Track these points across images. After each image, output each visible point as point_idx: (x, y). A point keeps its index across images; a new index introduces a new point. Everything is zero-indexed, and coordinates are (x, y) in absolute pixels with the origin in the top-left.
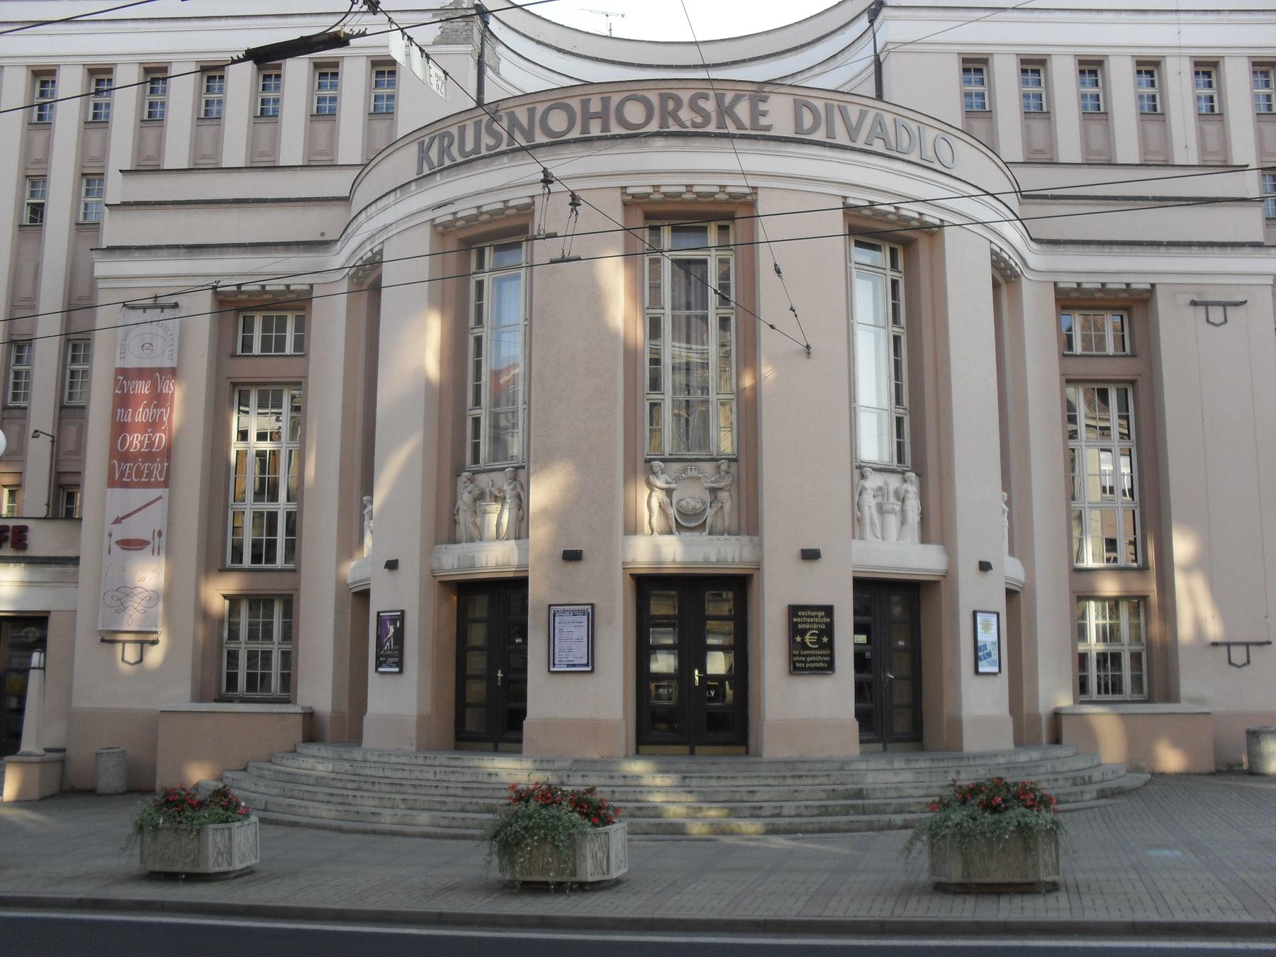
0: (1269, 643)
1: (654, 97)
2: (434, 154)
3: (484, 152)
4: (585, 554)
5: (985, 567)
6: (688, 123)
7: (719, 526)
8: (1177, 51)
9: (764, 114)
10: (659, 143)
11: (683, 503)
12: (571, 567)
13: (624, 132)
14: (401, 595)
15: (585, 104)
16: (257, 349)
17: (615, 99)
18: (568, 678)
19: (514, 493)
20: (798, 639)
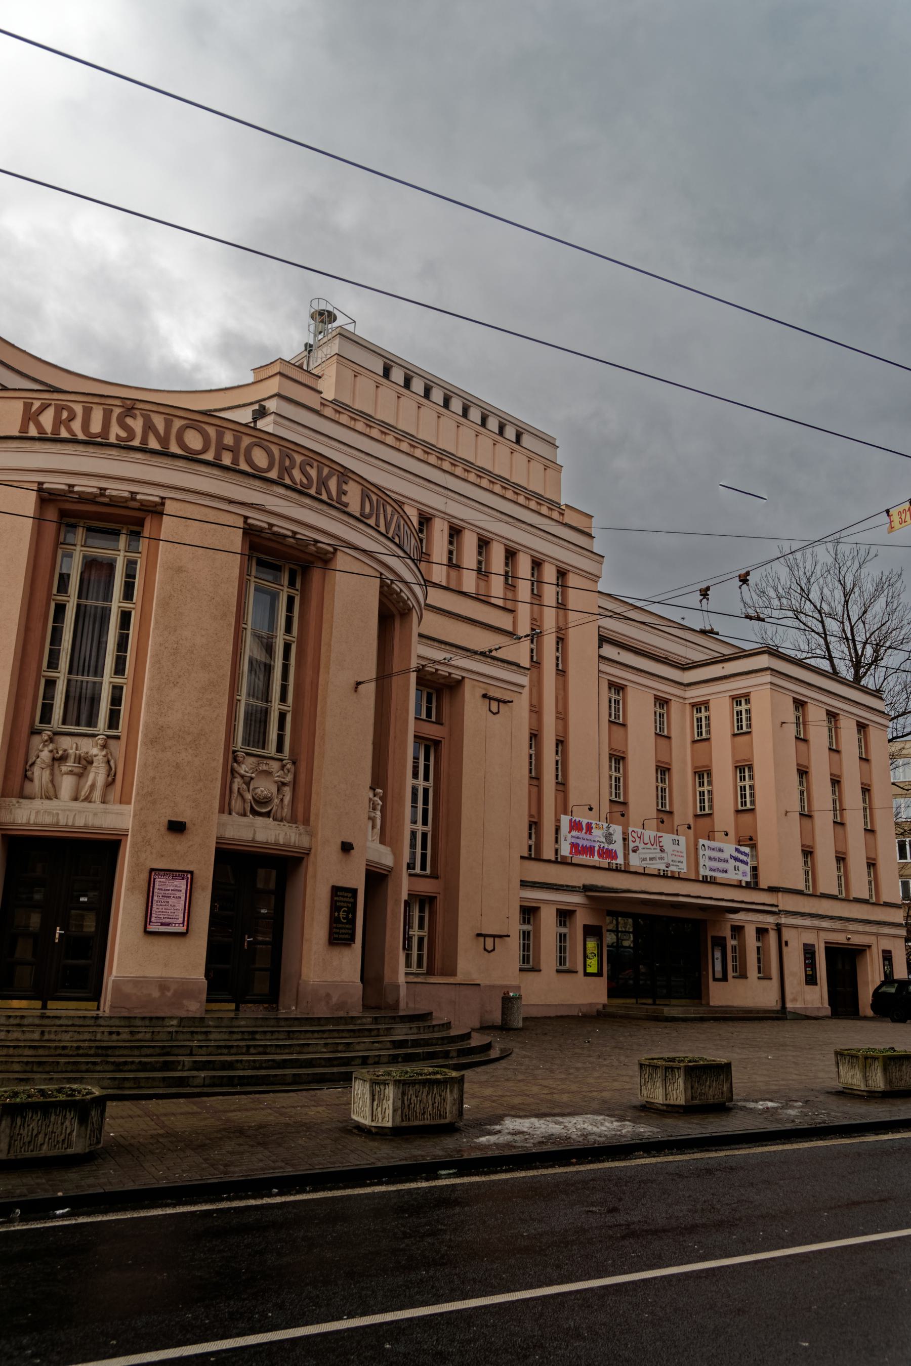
1: (275, 450)
2: (47, 419)
3: (112, 439)
4: (163, 829)
5: (347, 848)
8: (443, 515)
9: (345, 493)
10: (139, 456)
11: (258, 791)
12: (171, 838)
13: (179, 451)
15: (220, 436)
17: (246, 441)
18: (163, 941)
19: (105, 759)
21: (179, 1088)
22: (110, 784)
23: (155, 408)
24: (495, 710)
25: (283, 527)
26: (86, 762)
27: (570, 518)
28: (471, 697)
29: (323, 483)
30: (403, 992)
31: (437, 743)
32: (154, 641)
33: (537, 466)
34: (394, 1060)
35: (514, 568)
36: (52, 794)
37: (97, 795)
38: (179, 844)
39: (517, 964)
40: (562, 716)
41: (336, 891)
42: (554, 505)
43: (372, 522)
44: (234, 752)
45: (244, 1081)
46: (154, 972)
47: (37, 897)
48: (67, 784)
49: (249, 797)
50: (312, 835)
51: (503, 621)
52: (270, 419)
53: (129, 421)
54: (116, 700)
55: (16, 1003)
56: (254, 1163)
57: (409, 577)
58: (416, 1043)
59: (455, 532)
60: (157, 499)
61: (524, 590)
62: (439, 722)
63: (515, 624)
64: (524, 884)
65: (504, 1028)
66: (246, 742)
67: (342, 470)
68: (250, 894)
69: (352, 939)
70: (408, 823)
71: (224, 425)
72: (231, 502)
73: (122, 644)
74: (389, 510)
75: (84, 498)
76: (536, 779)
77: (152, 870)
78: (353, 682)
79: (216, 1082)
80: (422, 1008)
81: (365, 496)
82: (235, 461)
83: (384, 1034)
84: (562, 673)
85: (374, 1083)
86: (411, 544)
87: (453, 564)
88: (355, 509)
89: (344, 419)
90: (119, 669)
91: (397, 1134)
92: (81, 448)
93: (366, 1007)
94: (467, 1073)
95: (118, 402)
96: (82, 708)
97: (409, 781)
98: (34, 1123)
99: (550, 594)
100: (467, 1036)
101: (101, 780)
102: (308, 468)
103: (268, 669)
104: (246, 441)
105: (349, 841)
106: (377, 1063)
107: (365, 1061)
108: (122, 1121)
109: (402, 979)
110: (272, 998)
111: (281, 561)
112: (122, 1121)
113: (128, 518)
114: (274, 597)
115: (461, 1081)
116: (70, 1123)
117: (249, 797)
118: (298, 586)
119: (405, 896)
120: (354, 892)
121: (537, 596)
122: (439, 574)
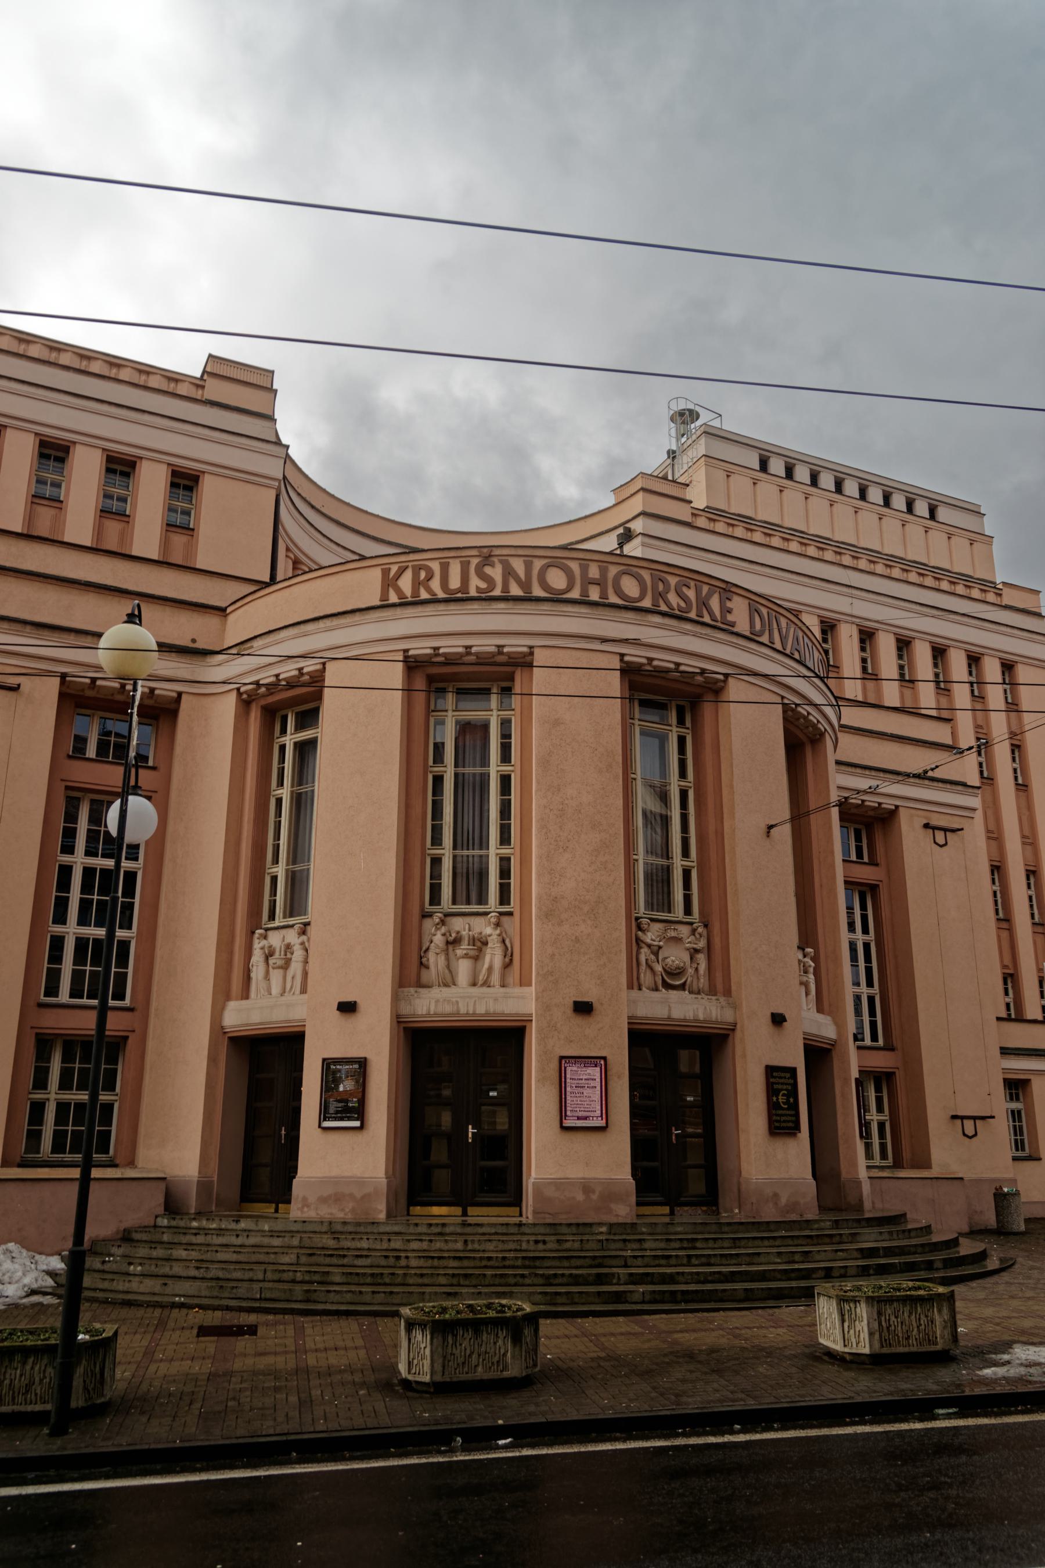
0: (993, 1117)
1: (646, 575)
2: (406, 583)
3: (473, 593)
4: (362, 1006)
5: (778, 1020)
6: (675, 606)
7: (695, 987)
9: (730, 611)
10: (502, 605)
13: (620, 602)
14: (374, 1041)
15: (584, 569)
16: (91, 752)
17: (613, 571)
20: (775, 1099)
21: (616, 1305)
22: (507, 965)
23: (513, 552)
24: (942, 841)
25: (664, 660)
26: (480, 943)
27: (1009, 597)
28: (910, 831)
29: (703, 604)
30: (866, 1188)
31: (874, 888)
32: (536, 804)
33: (960, 543)
34: (864, 1272)
35: (946, 670)
36: (449, 981)
37: (496, 978)
38: (587, 1027)
39: (1009, 1152)
40: (1030, 840)
41: (771, 1071)
42: (988, 585)
43: (765, 639)
44: (637, 919)
45: (688, 1297)
46: (576, 1172)
47: (447, 1093)
48: (463, 968)
49: (659, 968)
50: (735, 1007)
51: (940, 733)
52: (637, 541)
53: (488, 570)
54: (505, 873)
55: (436, 1210)
56: (707, 1394)
57: (818, 699)
58: (889, 1252)
59: (867, 637)
60: (525, 650)
61: (962, 696)
62: (873, 863)
63: (954, 734)
64: (1006, 1052)
65: (1001, 1232)
66: (650, 905)
67: (723, 585)
68: (673, 1079)
69: (797, 1127)
70: (849, 984)
71: (588, 558)
72: (604, 640)
73: (505, 811)
74: (783, 622)
75: (451, 660)
76: (1005, 920)
77: (562, 1058)
78: (764, 829)
79: (657, 1298)
80: (893, 1208)
81: (753, 611)
82: (604, 595)
83: (839, 1240)
84: (1023, 787)
85: (842, 1300)
86: (814, 658)
87: (869, 674)
88: (743, 627)
89: (720, 527)
90: (505, 838)
91: (876, 1362)
92: (442, 607)
93: (822, 1208)
94: (959, 1289)
95: (474, 552)
96: (471, 884)
97: (845, 936)
98: (466, 1341)
99: (995, 696)
100: (954, 1243)
101: (498, 961)
102: (685, 589)
103: (665, 820)
104: (613, 571)
105: (780, 1011)
106: (844, 1276)
107: (828, 1274)
108: (556, 1340)
109: (863, 1174)
110: (711, 1198)
111: (667, 699)
112: (556, 1340)
113: (498, 674)
114: (663, 740)
115: (951, 1298)
116: (502, 1344)
117: (659, 968)
118: (688, 724)
119: (855, 1074)
120: (793, 1071)
121: (978, 697)
122: (853, 689)
